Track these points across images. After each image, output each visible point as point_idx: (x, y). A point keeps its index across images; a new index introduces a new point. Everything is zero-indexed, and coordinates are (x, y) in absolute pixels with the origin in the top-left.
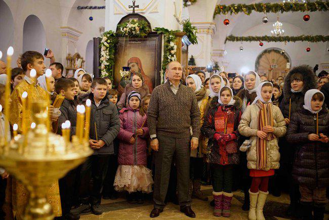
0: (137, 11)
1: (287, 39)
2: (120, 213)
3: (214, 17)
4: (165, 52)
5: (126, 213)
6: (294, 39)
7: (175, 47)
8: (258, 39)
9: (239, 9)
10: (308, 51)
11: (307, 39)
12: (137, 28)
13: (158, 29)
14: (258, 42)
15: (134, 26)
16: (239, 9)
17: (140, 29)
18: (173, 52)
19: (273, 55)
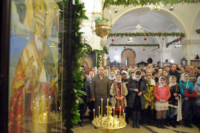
0: (86, 42)
1: (135, 45)
2: (87, 127)
3: (107, 38)
4: (98, 59)
5: (89, 127)
6: (138, 45)
7: (101, 57)
8: (123, 45)
9: (118, 35)
10: (144, 50)
11: (143, 45)
12: (86, 50)
13: (95, 50)
14: (123, 47)
15: (85, 49)
16: (118, 35)
17: (88, 50)
18: (101, 59)
19: (128, 51)
